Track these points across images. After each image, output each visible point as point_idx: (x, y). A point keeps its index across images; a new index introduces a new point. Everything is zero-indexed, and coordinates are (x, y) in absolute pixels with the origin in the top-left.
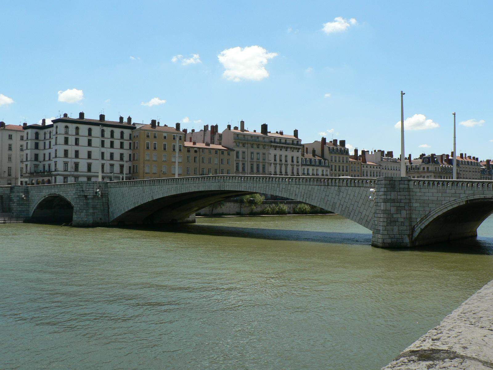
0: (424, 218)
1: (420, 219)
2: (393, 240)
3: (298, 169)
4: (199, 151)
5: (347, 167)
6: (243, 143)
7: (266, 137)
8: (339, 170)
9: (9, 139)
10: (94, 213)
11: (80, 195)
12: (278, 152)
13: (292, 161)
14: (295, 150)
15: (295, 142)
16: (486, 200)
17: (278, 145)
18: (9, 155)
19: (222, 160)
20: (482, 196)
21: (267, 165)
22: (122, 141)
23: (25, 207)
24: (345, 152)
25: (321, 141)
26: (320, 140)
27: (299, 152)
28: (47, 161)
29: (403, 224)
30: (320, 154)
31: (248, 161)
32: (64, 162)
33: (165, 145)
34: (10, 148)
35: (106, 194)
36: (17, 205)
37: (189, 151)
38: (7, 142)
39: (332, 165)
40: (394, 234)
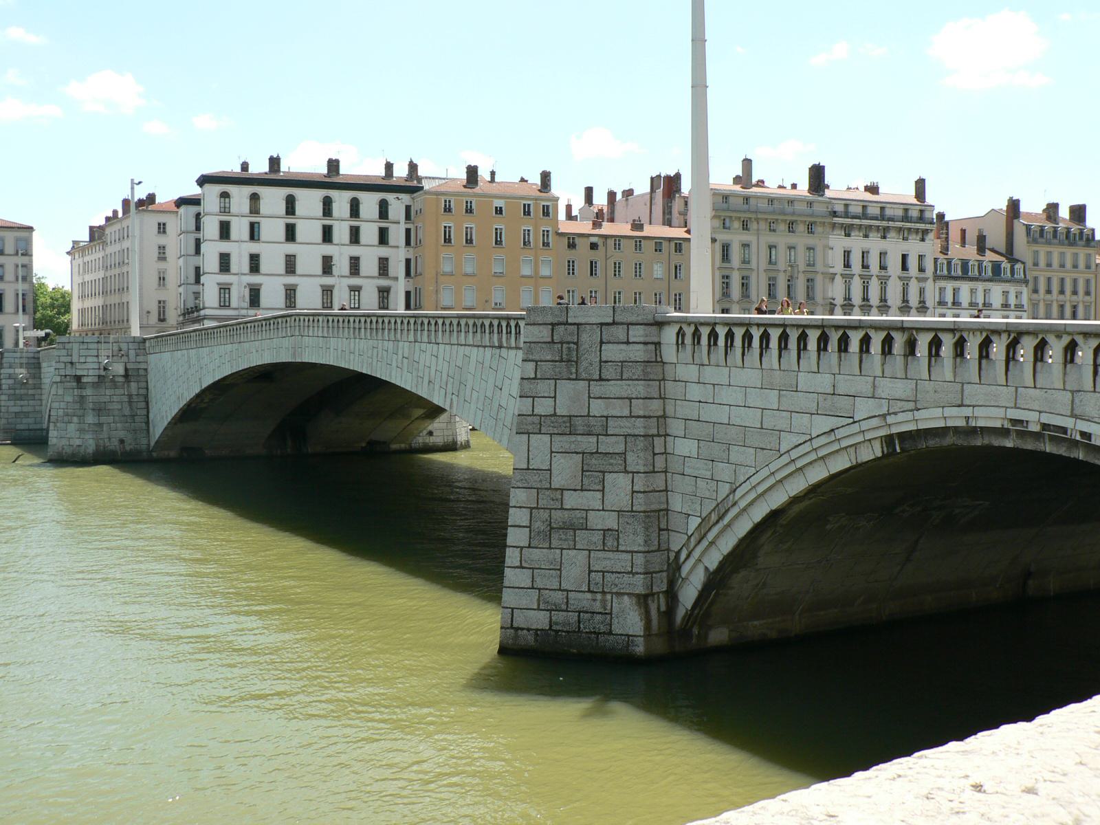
0: (714, 517)
1: (699, 520)
2: (559, 617)
3: (922, 292)
4: (605, 244)
5: (1088, 281)
6: (742, 219)
7: (820, 202)
8: (1062, 292)
9: (159, 232)
10: (100, 425)
11: (66, 376)
12: (856, 243)
13: (904, 267)
14: (912, 236)
15: (914, 213)
16: (979, 442)
17: (856, 221)
18: (159, 273)
19: (676, 267)
20: (955, 417)
21: (819, 280)
22: (384, 225)
23: (31, 402)
24: (1081, 238)
25: (1005, 209)
26: (1003, 205)
27: (927, 241)
28: (10, 282)
29: (610, 542)
30: (1001, 246)
31: (758, 269)
32: (218, 284)
33: (498, 233)
34: (162, 257)
35: (142, 372)
36: (7, 398)
37: (572, 246)
38: (155, 240)
39: (1036, 279)
40: (564, 586)
